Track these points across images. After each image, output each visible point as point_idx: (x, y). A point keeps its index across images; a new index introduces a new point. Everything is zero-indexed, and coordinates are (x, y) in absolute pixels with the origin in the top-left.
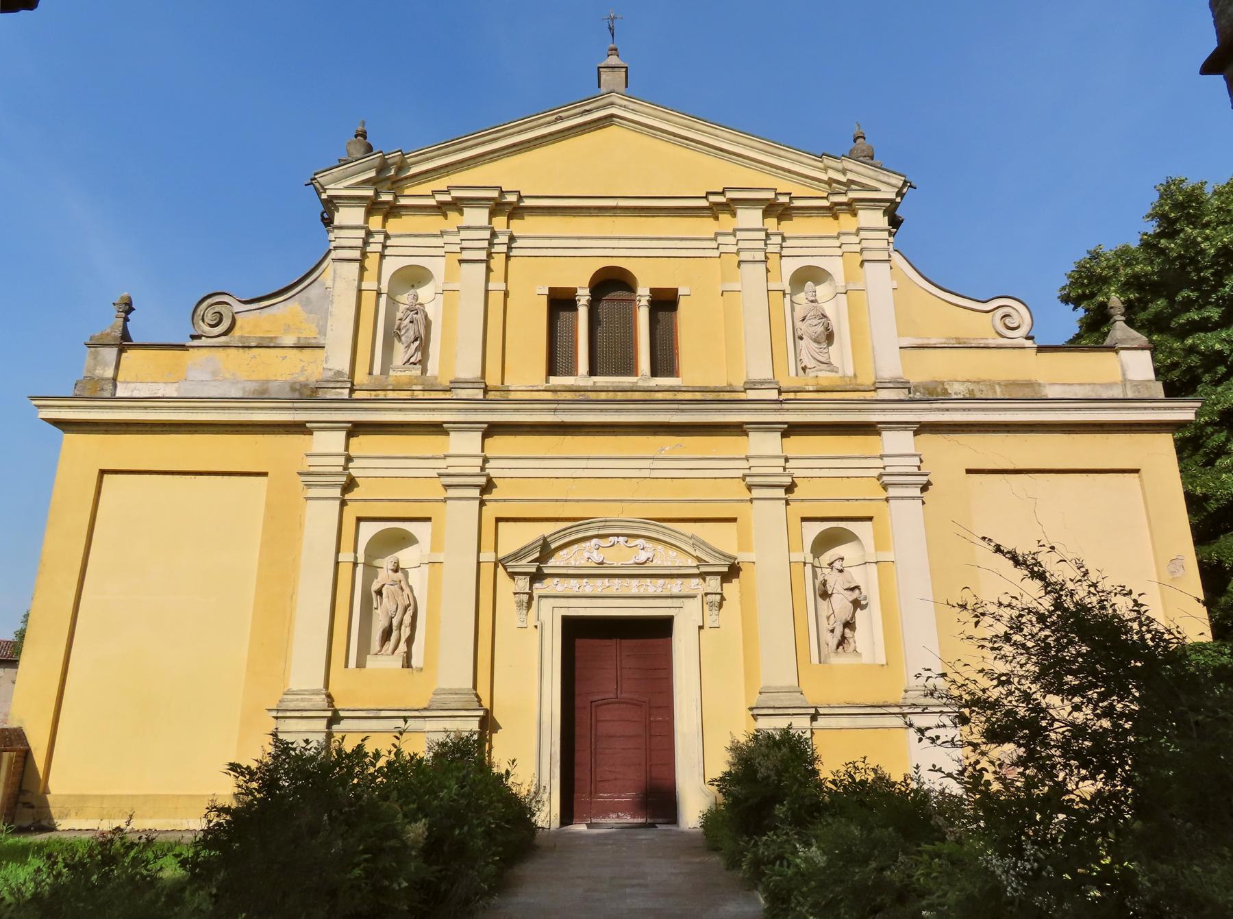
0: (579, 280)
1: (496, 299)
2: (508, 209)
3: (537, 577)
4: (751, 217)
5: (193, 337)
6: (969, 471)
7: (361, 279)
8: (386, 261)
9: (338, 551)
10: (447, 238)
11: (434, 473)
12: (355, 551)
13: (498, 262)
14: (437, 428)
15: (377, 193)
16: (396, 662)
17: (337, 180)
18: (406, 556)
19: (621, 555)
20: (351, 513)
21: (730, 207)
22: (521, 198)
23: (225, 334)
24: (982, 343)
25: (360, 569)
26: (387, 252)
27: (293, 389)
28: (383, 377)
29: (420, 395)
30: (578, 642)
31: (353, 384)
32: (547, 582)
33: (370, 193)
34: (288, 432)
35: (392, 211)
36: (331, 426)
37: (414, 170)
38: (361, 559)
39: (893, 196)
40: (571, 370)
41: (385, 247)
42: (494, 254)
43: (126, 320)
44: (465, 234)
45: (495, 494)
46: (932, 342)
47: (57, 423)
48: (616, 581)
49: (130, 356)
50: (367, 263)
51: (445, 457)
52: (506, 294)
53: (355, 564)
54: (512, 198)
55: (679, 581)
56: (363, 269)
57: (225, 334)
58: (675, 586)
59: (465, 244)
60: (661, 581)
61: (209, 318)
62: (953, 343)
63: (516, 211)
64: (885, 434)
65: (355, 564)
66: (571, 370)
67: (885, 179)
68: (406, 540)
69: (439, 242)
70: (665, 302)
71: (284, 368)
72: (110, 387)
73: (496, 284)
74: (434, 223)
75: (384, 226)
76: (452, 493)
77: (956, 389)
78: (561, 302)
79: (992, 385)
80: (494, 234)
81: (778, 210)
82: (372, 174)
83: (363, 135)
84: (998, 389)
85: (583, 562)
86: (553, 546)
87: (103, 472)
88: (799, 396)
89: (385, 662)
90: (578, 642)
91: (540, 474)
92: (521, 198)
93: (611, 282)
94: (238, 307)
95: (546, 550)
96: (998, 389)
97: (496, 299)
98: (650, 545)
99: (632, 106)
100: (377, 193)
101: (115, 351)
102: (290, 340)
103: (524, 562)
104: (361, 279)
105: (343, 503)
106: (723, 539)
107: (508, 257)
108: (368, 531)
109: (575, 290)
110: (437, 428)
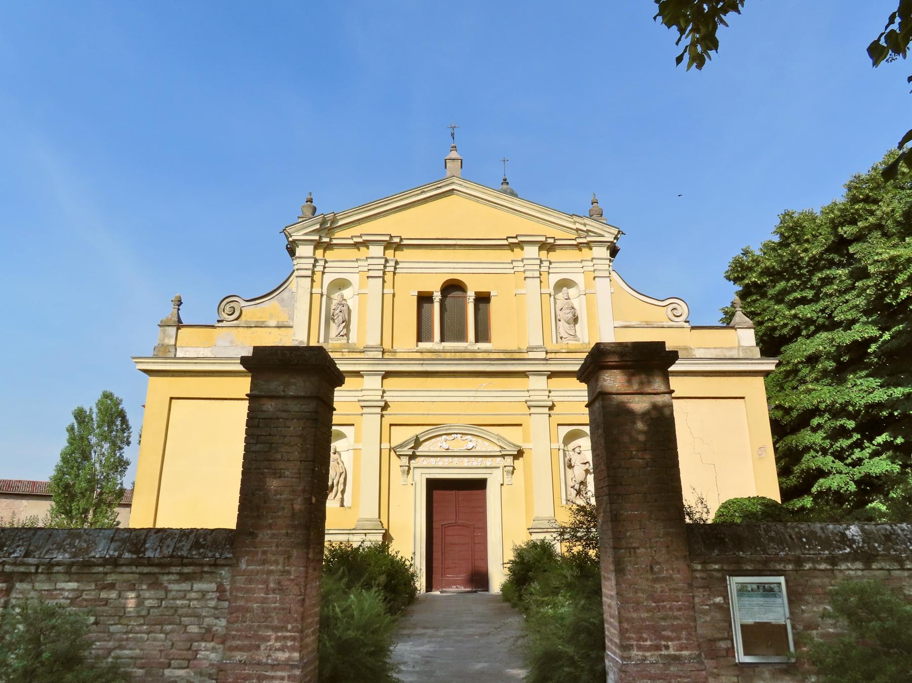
0: (435, 287)
1: (388, 299)
3: (412, 457)
4: (532, 251)
5: (219, 321)
10: (360, 263)
13: (389, 277)
17: (298, 231)
19: (459, 444)
21: (521, 245)
22: (401, 239)
23: (237, 319)
24: (661, 324)
29: (347, 355)
30: (435, 492)
32: (418, 459)
35: (329, 246)
37: (340, 223)
41: (325, 267)
42: (387, 273)
45: (389, 411)
46: (633, 323)
47: (146, 371)
48: (456, 459)
52: (394, 295)
55: (490, 459)
57: (237, 319)
58: (488, 462)
59: (371, 267)
60: (480, 459)
62: (644, 324)
69: (356, 264)
70: (483, 299)
73: (388, 290)
76: (366, 410)
78: (424, 299)
81: (547, 246)
82: (318, 226)
85: (438, 449)
87: (171, 398)
92: (401, 239)
93: (453, 287)
97: (388, 299)
98: (474, 439)
99: (465, 184)
100: (320, 237)
101: (175, 329)
102: (273, 323)
103: (406, 449)
106: (514, 436)
107: (394, 273)
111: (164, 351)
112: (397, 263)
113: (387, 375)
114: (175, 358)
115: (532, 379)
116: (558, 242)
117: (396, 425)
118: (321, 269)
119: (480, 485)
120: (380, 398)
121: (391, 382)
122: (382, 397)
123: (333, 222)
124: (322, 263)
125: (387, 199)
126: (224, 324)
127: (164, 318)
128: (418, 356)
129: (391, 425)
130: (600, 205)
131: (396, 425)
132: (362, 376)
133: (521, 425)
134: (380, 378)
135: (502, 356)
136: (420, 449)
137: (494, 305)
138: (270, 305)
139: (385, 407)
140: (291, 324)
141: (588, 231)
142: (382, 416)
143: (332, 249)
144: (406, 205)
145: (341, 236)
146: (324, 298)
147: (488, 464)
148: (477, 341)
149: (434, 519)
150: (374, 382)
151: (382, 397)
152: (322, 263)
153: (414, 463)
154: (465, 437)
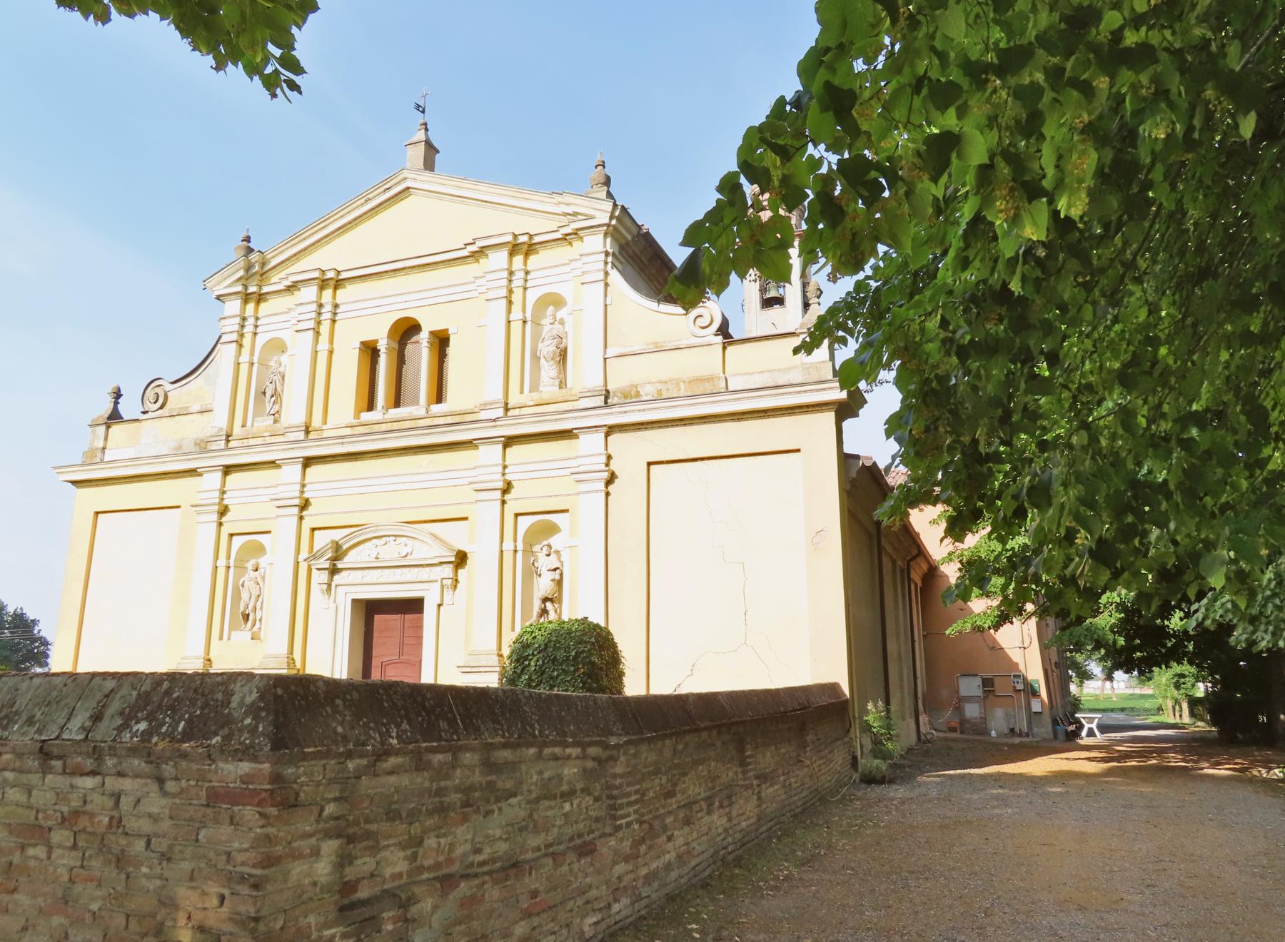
0: (380, 333)
1: (322, 358)
2: (332, 283)
3: (334, 571)
4: (499, 259)
5: (144, 413)
6: (798, 451)
7: (509, 311)
8: (529, 292)
9: (502, 541)
10: (574, 265)
11: (567, 472)
12: (515, 541)
13: (325, 328)
14: (272, 464)
15: (246, 287)
16: (249, 635)
17: (219, 283)
18: (556, 541)
19: (390, 551)
20: (226, 530)
21: (482, 252)
22: (515, 236)
23: (161, 408)
24: (676, 344)
25: (519, 555)
26: (259, 330)
27: (196, 444)
28: (564, 390)
29: (269, 440)
30: (377, 617)
31: (506, 404)
32: (344, 573)
33: (239, 288)
34: (416, 453)
35: (261, 298)
36: (488, 440)
37: (273, 263)
38: (520, 546)
39: (607, 221)
40: (415, 401)
41: (256, 326)
42: (323, 322)
43: (116, 403)
44: (585, 259)
45: (311, 510)
46: (636, 349)
47: (74, 483)
48: (386, 571)
49: (116, 429)
50: (514, 298)
51: (475, 468)
52: (331, 352)
53: (516, 551)
54: (331, 275)
55: (427, 569)
56: (510, 303)
57: (161, 408)
58: (424, 574)
59: (301, 317)
60: (416, 570)
61: (152, 399)
62: (652, 348)
63: (338, 284)
64: (205, 475)
65: (516, 551)
66: (415, 401)
67: (598, 207)
68: (553, 529)
69: (567, 269)
70: (441, 341)
71: (192, 428)
72: (99, 454)
73: (323, 345)
74: (562, 252)
75: (525, 264)
76: (583, 487)
77: (647, 391)
78: (370, 351)
79: (677, 382)
80: (511, 273)
81: (523, 248)
82: (241, 273)
83: (248, 239)
84: (682, 386)
85: (367, 559)
86: (345, 547)
87: (649, 464)
88: (524, 411)
89: (242, 636)
90: (377, 617)
91: (341, 494)
92: (531, 236)
93: (406, 330)
94: (168, 387)
95: (338, 552)
96: (682, 386)
97: (322, 358)
98: (410, 542)
99: (418, 177)
100: (246, 287)
101: (103, 428)
102: (196, 408)
103: (322, 560)
104: (509, 311)
105: (504, 502)
106: (457, 537)
107: (334, 321)
108: (525, 523)
109: (376, 341)
110: (272, 464)
111: (96, 455)
112: (336, 306)
113: (509, 441)
114: (727, 391)
115: (483, 449)
116: (537, 239)
117: (319, 529)
118: (521, 283)
119: (414, 606)
120: (603, 467)
121: (515, 451)
122: (607, 465)
123: (263, 264)
124: (521, 275)
125: (324, 220)
126: (150, 415)
127: (95, 416)
128: (348, 431)
129: (517, 515)
130: (608, 171)
131: (319, 529)
132: (279, 466)
133: (567, 511)
134: (500, 447)
135: (449, 420)
136: (346, 559)
137: (452, 350)
138: (195, 383)
139: (305, 505)
140: (209, 407)
141: (575, 214)
142: (504, 502)
143: (266, 300)
144: (345, 225)
145: (277, 281)
146: (529, 326)
147: (425, 578)
148: (397, 404)
149: (374, 653)
150: (591, 443)
151: (607, 465)
152: (522, 274)
153: (337, 579)
154: (399, 540)
